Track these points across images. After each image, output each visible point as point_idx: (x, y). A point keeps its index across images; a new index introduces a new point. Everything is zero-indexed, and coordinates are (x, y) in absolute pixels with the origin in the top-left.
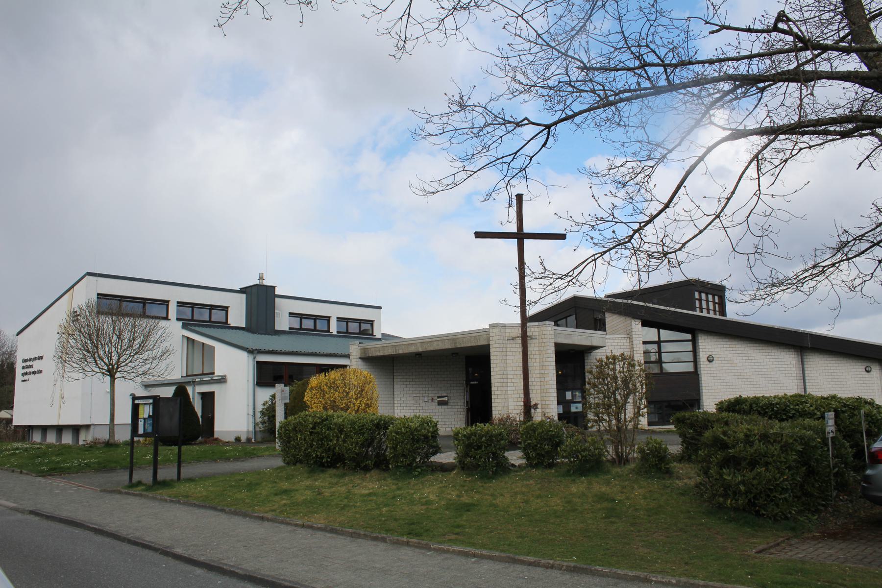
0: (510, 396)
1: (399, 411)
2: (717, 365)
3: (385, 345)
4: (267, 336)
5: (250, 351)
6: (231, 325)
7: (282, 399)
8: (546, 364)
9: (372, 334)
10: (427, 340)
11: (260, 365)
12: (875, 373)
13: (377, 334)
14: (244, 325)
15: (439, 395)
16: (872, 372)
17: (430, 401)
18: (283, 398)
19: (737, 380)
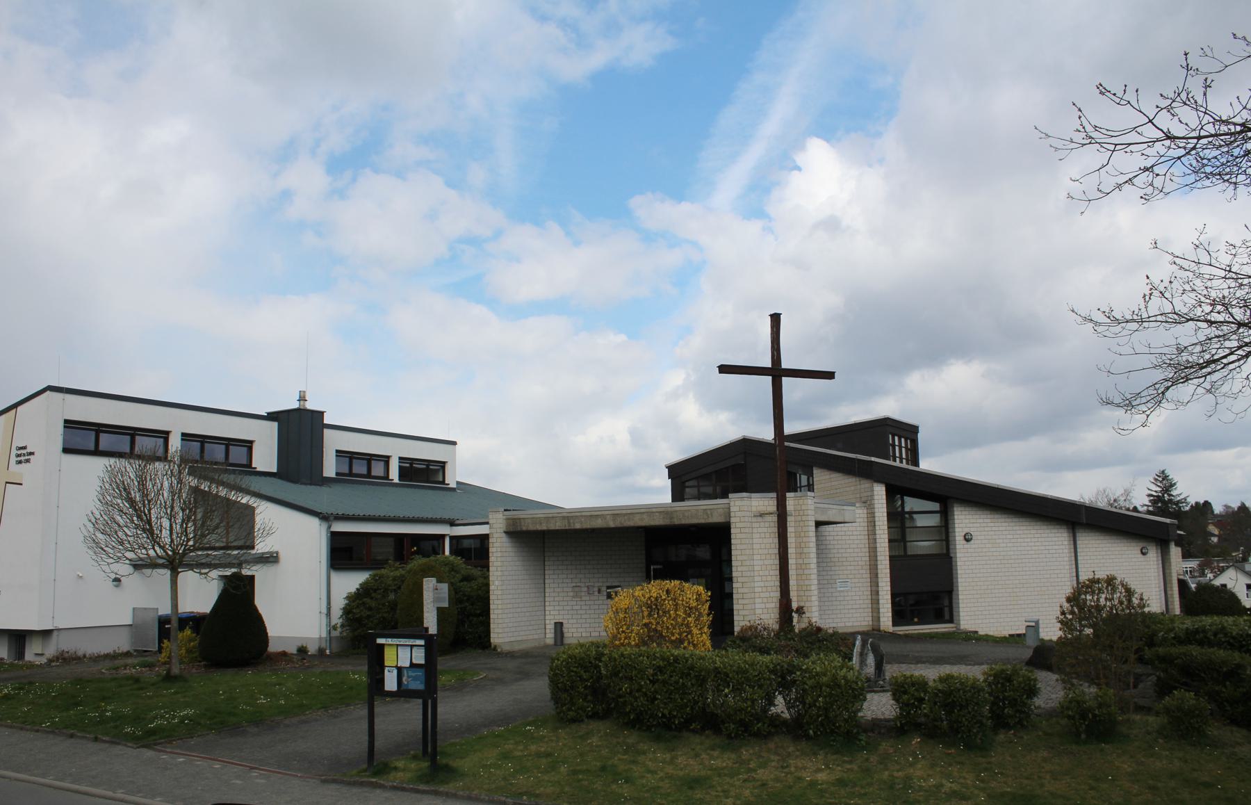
0: (757, 595)
1: (552, 608)
2: (976, 546)
3: (551, 515)
4: (313, 487)
5: (324, 517)
6: (258, 470)
7: (433, 602)
8: (805, 550)
9: (443, 482)
10: (624, 512)
11: (334, 536)
12: (1151, 555)
13: (451, 481)
14: (275, 470)
15: (609, 584)
16: (1148, 555)
17: (596, 593)
18: (436, 600)
19: (1000, 566)
